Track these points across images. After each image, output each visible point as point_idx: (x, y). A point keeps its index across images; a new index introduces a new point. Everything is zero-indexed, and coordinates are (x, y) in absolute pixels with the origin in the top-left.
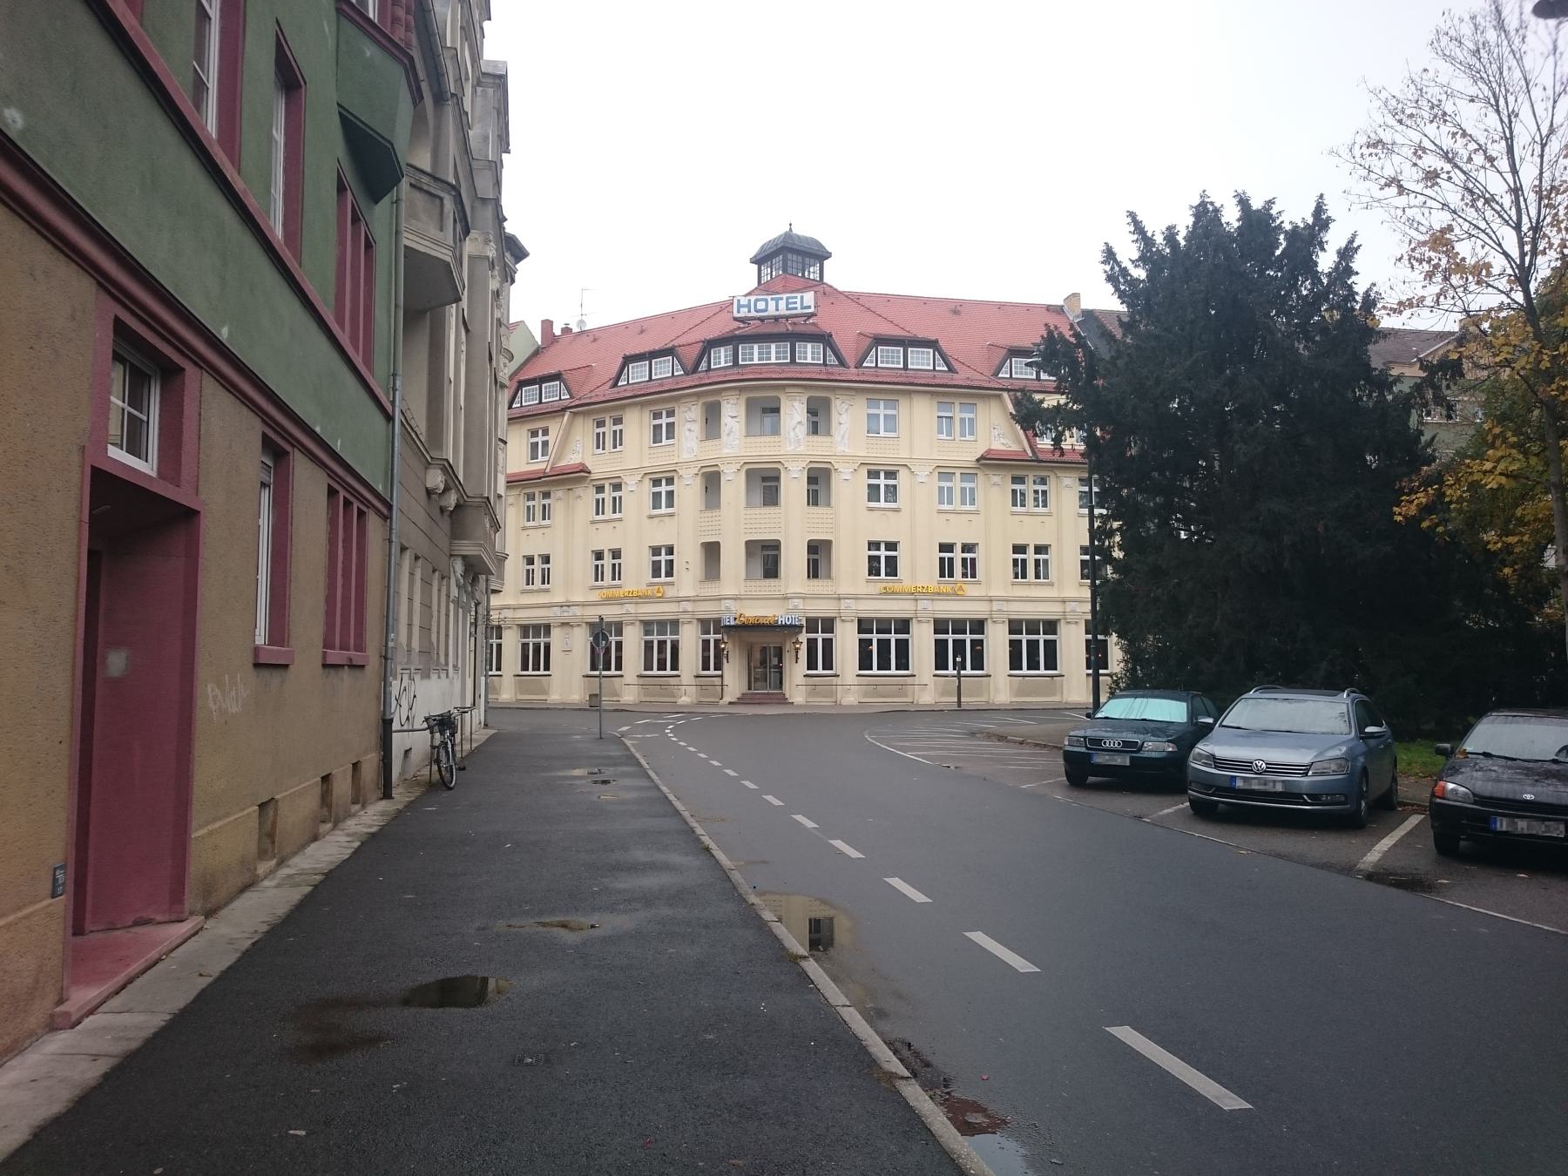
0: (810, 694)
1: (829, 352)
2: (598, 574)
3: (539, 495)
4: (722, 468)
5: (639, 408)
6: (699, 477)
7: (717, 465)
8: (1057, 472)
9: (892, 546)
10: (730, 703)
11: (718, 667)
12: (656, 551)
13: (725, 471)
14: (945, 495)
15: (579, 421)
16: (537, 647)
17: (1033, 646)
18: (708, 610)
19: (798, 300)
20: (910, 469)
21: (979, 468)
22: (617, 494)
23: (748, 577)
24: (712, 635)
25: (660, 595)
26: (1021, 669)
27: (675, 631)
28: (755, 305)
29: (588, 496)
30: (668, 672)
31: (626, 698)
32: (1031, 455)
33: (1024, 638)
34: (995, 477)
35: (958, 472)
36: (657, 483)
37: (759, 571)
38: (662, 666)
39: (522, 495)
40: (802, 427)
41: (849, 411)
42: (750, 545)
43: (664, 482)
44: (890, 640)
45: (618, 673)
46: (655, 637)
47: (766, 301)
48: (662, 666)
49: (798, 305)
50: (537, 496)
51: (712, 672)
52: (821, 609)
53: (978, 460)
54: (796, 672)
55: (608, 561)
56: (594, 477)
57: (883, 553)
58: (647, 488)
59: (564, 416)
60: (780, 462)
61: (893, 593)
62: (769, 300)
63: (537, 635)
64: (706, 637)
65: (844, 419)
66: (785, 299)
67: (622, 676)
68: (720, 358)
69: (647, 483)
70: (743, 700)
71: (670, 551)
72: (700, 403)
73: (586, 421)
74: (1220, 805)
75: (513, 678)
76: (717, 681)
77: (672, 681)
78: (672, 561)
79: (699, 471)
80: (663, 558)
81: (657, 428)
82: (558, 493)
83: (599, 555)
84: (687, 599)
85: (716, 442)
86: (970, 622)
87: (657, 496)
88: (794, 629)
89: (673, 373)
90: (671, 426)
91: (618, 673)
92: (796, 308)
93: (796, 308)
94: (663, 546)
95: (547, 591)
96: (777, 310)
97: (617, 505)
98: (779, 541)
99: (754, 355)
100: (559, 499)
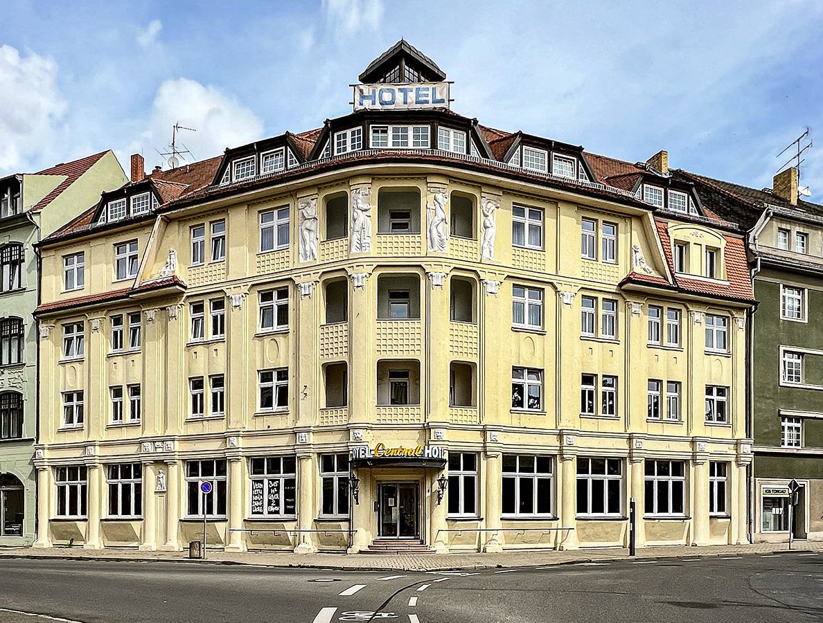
0: (451, 540)
1: (473, 146)
3: (128, 317)
4: (350, 271)
5: (177, 223)
7: (343, 269)
9: (283, 374)
10: (361, 552)
11: (344, 508)
12: (266, 376)
14: (589, 322)
15: (174, 227)
16: (73, 489)
17: (526, 484)
18: (333, 442)
19: (430, 93)
20: (556, 288)
22: (218, 312)
23: (380, 403)
24: (606, 475)
27: (221, 472)
28: (380, 98)
29: (183, 313)
32: (671, 283)
35: (600, 296)
37: (388, 397)
39: (108, 318)
42: (382, 365)
43: (275, 294)
46: (517, 473)
47: (393, 92)
49: (430, 99)
50: (124, 318)
51: (336, 515)
52: (469, 441)
53: (621, 285)
54: (437, 516)
55: (208, 390)
56: (188, 292)
58: (255, 301)
59: (153, 224)
60: (420, 266)
62: (397, 91)
66: (414, 91)
68: (345, 143)
69: (255, 298)
70: (373, 550)
73: (181, 228)
74: (385, 522)
76: (344, 526)
80: (275, 382)
81: (267, 232)
82: (150, 313)
83: (198, 383)
87: (266, 312)
88: (432, 466)
89: (286, 166)
90: (284, 229)
92: (427, 102)
93: (427, 102)
95: (137, 425)
96: (405, 103)
97: (219, 325)
99: (387, 140)
100: (151, 320)
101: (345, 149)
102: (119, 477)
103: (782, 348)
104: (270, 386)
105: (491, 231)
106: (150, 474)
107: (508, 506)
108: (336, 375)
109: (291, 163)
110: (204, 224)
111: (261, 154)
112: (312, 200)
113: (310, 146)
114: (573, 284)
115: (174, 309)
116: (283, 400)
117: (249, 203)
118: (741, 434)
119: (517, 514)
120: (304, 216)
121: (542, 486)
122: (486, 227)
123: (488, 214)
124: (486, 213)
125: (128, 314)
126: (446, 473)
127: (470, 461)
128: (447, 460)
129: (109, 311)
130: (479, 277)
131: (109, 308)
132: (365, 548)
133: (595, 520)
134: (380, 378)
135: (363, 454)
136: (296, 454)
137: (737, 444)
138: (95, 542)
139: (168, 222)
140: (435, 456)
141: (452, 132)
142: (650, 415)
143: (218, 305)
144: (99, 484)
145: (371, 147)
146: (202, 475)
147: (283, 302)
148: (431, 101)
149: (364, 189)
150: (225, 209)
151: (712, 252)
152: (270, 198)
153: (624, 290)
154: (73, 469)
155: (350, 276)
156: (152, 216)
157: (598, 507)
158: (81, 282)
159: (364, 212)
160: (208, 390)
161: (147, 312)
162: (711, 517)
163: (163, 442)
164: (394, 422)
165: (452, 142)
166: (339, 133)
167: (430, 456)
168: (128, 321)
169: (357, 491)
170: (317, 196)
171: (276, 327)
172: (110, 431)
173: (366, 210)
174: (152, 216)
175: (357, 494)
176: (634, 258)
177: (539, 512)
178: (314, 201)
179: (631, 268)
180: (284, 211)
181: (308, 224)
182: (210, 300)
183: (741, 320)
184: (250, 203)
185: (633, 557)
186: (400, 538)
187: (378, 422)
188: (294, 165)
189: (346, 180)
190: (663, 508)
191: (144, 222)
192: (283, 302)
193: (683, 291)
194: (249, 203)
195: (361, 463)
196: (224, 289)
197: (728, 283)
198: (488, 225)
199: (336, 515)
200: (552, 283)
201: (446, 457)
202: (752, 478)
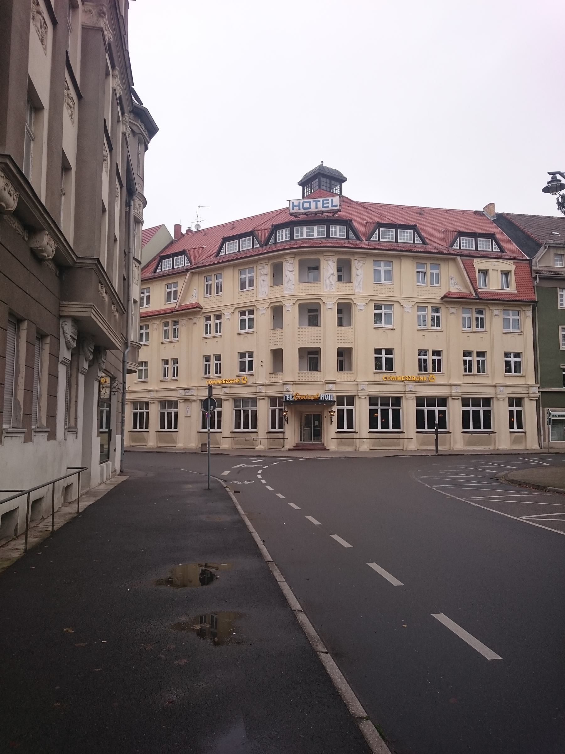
0: (339, 444)
1: (350, 232)
3: (172, 323)
4: (284, 303)
5: (198, 275)
10: (289, 450)
11: (282, 426)
15: (196, 278)
18: (275, 391)
19: (330, 202)
20: (400, 304)
22: (218, 321)
25: (245, 382)
30: (250, 430)
33: (471, 409)
36: (243, 313)
37: (306, 366)
39: (162, 323)
47: (310, 202)
49: (330, 205)
51: (277, 430)
52: (346, 390)
53: (442, 298)
55: (213, 362)
56: (204, 311)
57: (247, 359)
58: (237, 317)
59: (186, 275)
61: (390, 381)
64: (274, 408)
68: (282, 236)
70: (297, 448)
76: (281, 436)
77: (253, 435)
79: (269, 305)
82: (183, 321)
88: (330, 403)
92: (328, 207)
95: (176, 380)
97: (218, 328)
99: (303, 233)
101: (282, 239)
102: (166, 409)
103: (560, 327)
104: (245, 360)
105: (359, 278)
106: (181, 406)
107: (466, 425)
108: (277, 355)
109: (256, 245)
110: (211, 275)
112: (265, 265)
113: (266, 234)
114: (291, 299)
115: (196, 319)
116: (251, 368)
118: (532, 381)
119: (471, 430)
120: (261, 273)
122: (357, 275)
123: (358, 268)
124: (357, 268)
125: (172, 321)
126: (335, 408)
127: (350, 400)
128: (336, 401)
129: (162, 319)
130: (353, 302)
131: (163, 318)
132: (291, 448)
133: (428, 433)
134: (301, 357)
135: (288, 398)
136: (257, 397)
137: (528, 387)
138: (152, 442)
139: (193, 274)
140: (326, 399)
141: (338, 227)
142: (465, 371)
143: (219, 317)
144: (154, 412)
145: (295, 238)
147: (251, 316)
148: (330, 206)
149: (290, 260)
150: (222, 268)
151: (506, 273)
153: (444, 301)
154: (141, 403)
155: (284, 305)
156: (187, 270)
157: (385, 425)
158: (148, 303)
159: (291, 272)
160: (213, 362)
162: (511, 432)
164: (301, 380)
165: (338, 232)
166: (279, 231)
167: (324, 399)
168: (162, 364)
169: (288, 417)
170: (267, 263)
171: (247, 330)
172: (465, 377)
173: (292, 271)
174: (187, 270)
175: (287, 419)
176: (450, 282)
177: (243, 428)
178: (266, 266)
179: (449, 289)
181: (263, 278)
182: (214, 315)
183: (529, 313)
184: (234, 266)
185: (437, 454)
186: (313, 442)
187: (299, 381)
189: (282, 256)
190: (477, 426)
191: (182, 273)
192: (251, 316)
193: (481, 299)
195: (288, 403)
196: (221, 309)
197: (516, 292)
198: (358, 274)
199: (277, 430)
200: (398, 301)
201: (335, 399)
202: (541, 408)
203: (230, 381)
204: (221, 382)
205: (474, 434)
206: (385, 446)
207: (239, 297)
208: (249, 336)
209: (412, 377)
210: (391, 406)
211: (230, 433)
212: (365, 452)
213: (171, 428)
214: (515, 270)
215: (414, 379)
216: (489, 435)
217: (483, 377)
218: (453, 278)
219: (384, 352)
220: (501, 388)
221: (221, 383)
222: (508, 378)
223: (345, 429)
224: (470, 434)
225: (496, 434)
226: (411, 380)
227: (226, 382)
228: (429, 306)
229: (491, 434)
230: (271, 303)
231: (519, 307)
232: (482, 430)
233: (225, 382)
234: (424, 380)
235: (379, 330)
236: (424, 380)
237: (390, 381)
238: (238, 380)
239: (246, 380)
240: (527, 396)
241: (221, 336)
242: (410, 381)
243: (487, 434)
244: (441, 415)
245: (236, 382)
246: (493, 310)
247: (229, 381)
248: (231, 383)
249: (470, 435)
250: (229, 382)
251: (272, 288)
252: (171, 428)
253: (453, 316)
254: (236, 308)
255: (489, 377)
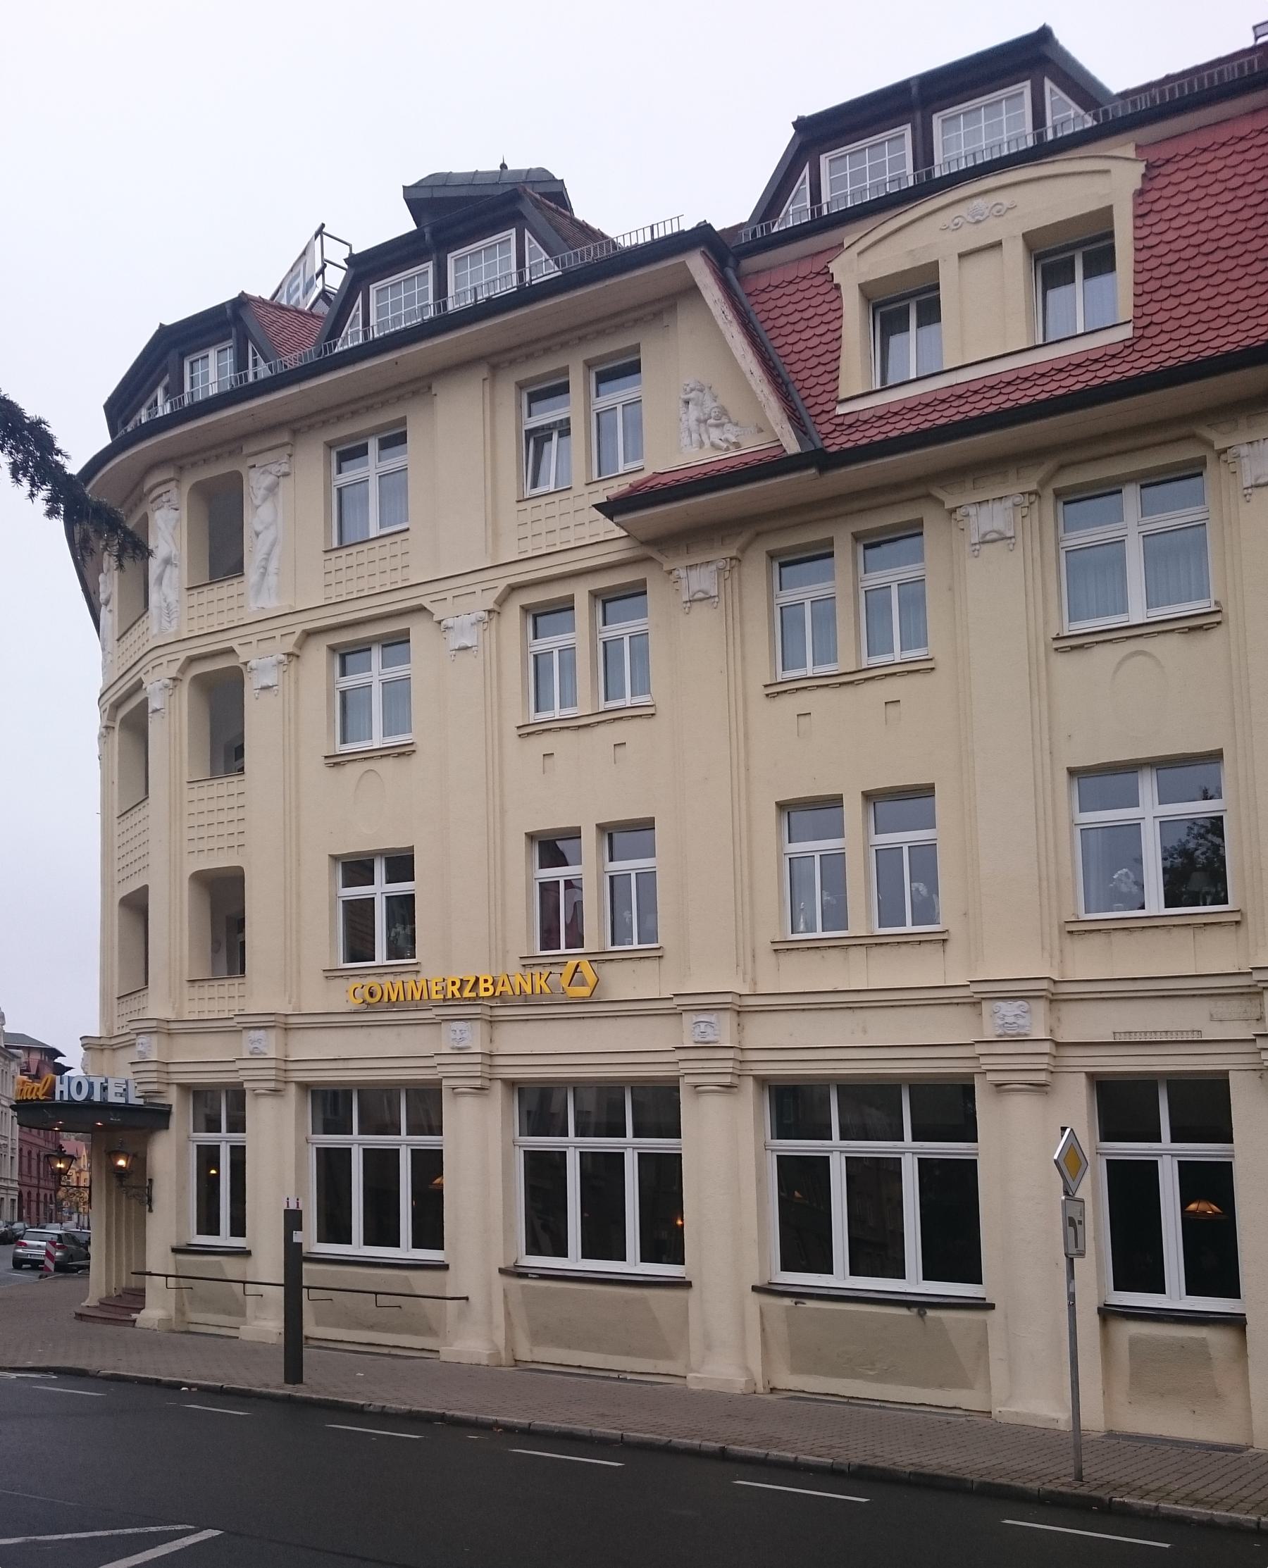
2: (359, 947)
4: (243, 654)
5: (484, 372)
6: (185, 689)
7: (231, 651)
8: (940, 494)
9: (401, 866)
13: (253, 663)
21: (647, 559)
25: (584, 991)
26: (396, 1244)
30: (405, 1251)
31: (458, 1346)
33: (357, 1143)
34: (694, 574)
36: (346, 656)
38: (381, 1231)
40: (176, 572)
41: (281, 491)
44: (826, 1160)
45: (237, 1242)
48: (381, 1231)
57: (380, 889)
61: (392, 1006)
63: (379, 1123)
64: (335, 1140)
65: (265, 512)
67: (444, 1267)
71: (401, 866)
72: (186, 487)
75: (171, 1255)
77: (422, 1282)
78: (409, 900)
79: (183, 670)
84: (708, 1005)
85: (934, 327)
86: (912, 1089)
91: (237, 1242)
94: (380, 853)
98: (241, 869)
111: (371, 286)
117: (297, 426)
121: (213, 1172)
146: (361, 1133)
152: (353, 407)
161: (972, 511)
163: (977, 1004)
167: (66, 1098)
172: (786, 959)
180: (394, 440)
188: (543, 268)
194: (297, 426)
196: (425, 602)
203: (488, 985)
204: (434, 989)
205: (811, 1304)
206: (371, 1327)
207: (331, 579)
208: (386, 767)
209: (477, 979)
210: (635, 1136)
211: (170, 1251)
212: (468, 1373)
213: (215, 1232)
214: (1140, 193)
215: (486, 990)
216: (922, 1315)
217: (904, 948)
218: (692, 395)
219: (380, 870)
220: (1009, 1010)
221: (434, 996)
222: (1098, 940)
223: (1175, 1296)
224: (788, 1302)
225: (991, 1313)
226: (473, 995)
227: (466, 994)
228: (580, 593)
229: (930, 1313)
230: (192, 660)
231: (1192, 437)
232: (574, 1261)
233: (460, 990)
234: (538, 991)
235: (349, 767)
236: (538, 991)
237: (392, 1006)
238: (539, 983)
239: (591, 978)
240: (1246, 1059)
241: (412, 744)
242: (469, 999)
243: (903, 1311)
244: (213, 1172)
245: (529, 991)
246: (962, 511)
247: (482, 985)
248: (493, 996)
249: (787, 1308)
250: (482, 994)
251: (196, 598)
252: (215, 1232)
253: (702, 613)
254: (309, 634)
255: (949, 946)
